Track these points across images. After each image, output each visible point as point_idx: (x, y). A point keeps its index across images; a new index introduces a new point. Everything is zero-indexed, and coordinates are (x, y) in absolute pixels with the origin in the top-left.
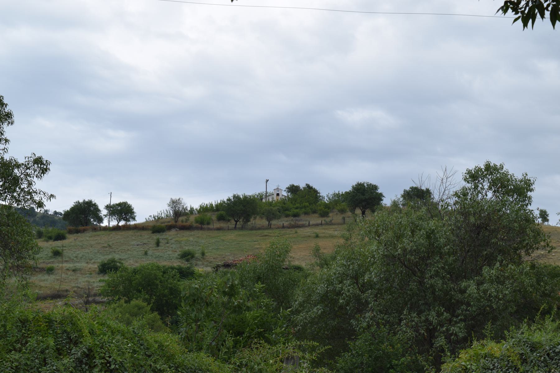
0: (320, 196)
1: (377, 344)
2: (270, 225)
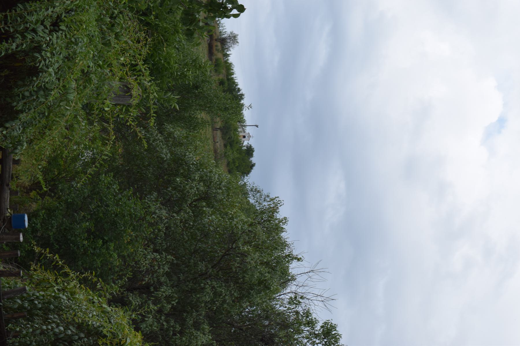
0: (244, 177)
1: (132, 224)
2: (216, 129)
